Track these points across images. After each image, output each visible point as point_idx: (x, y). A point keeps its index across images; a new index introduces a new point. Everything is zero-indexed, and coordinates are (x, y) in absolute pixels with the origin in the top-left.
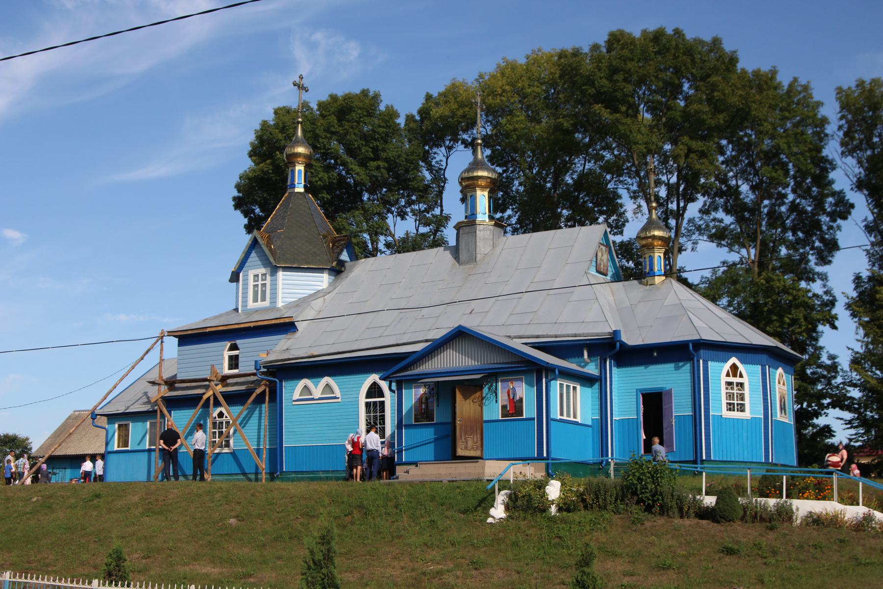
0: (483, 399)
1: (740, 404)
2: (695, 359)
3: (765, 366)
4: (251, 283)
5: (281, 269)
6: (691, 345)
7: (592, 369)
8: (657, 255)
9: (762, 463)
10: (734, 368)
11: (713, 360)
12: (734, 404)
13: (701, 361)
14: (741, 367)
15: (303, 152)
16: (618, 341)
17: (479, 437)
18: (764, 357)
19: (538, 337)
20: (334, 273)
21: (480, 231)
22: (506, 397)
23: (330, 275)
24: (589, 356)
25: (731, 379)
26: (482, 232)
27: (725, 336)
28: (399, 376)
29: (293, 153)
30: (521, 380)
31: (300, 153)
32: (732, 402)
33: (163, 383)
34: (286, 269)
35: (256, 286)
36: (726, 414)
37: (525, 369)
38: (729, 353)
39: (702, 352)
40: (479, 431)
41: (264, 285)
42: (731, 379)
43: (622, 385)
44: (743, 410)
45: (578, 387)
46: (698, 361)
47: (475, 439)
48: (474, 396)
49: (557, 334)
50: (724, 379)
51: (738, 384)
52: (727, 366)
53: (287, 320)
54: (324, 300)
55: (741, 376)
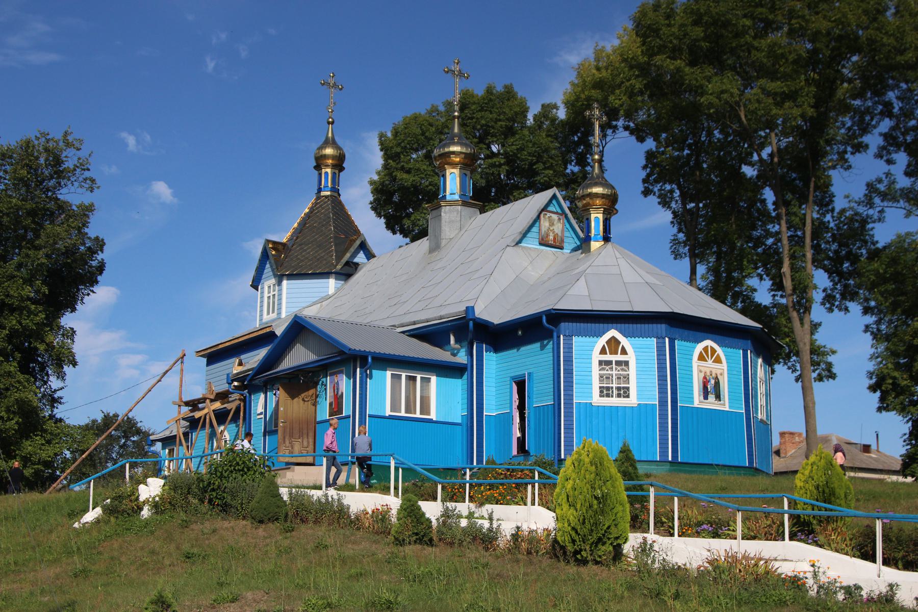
0: (317, 396)
1: (624, 388)
2: (555, 335)
3: (664, 338)
4: (266, 295)
5: (285, 278)
6: (544, 318)
7: (462, 358)
8: (593, 216)
9: (657, 461)
10: (613, 344)
11: (580, 334)
12: (612, 388)
13: (562, 336)
14: (624, 341)
15: (332, 153)
16: (471, 320)
17: (311, 440)
18: (662, 328)
19: (414, 323)
20: (343, 277)
21: (445, 213)
22: (332, 394)
23: (336, 279)
24: (457, 341)
25: (608, 357)
26: (448, 215)
27: (673, 308)
28: (267, 376)
29: (321, 156)
30: (341, 372)
31: (328, 155)
32: (611, 385)
33: (183, 404)
34: (291, 277)
35: (269, 297)
36: (597, 399)
37: (339, 358)
38: (606, 325)
39: (563, 326)
40: (311, 434)
41: (269, 292)
42: (608, 357)
43: (499, 373)
44: (628, 396)
45: (434, 379)
46: (559, 337)
47: (305, 444)
48: (306, 393)
49: (415, 320)
50: (597, 357)
51: (619, 363)
52: (603, 341)
53: (268, 330)
54: (321, 306)
55: (624, 352)
